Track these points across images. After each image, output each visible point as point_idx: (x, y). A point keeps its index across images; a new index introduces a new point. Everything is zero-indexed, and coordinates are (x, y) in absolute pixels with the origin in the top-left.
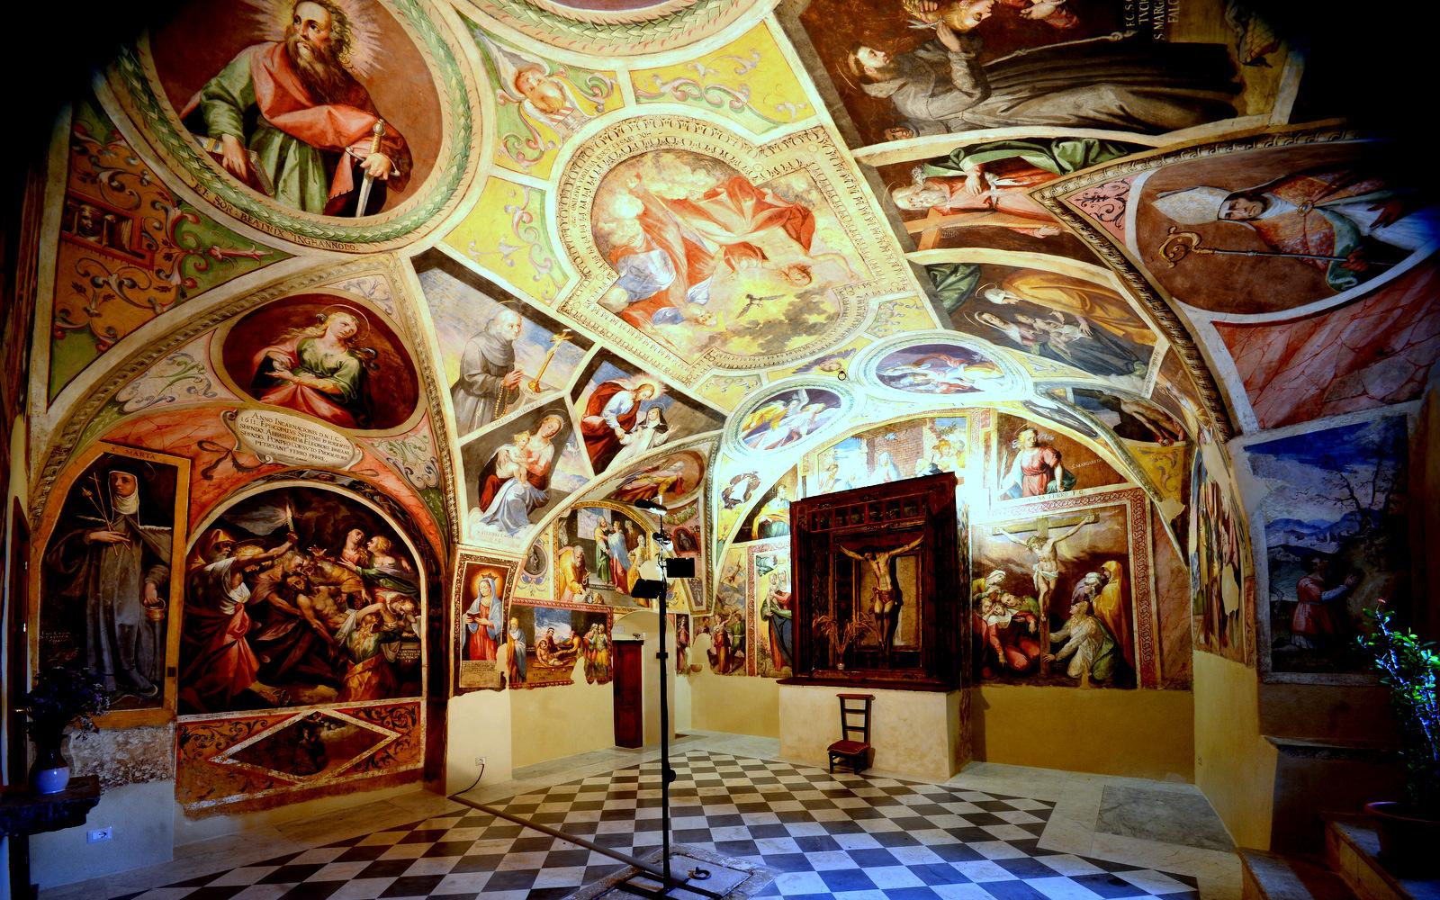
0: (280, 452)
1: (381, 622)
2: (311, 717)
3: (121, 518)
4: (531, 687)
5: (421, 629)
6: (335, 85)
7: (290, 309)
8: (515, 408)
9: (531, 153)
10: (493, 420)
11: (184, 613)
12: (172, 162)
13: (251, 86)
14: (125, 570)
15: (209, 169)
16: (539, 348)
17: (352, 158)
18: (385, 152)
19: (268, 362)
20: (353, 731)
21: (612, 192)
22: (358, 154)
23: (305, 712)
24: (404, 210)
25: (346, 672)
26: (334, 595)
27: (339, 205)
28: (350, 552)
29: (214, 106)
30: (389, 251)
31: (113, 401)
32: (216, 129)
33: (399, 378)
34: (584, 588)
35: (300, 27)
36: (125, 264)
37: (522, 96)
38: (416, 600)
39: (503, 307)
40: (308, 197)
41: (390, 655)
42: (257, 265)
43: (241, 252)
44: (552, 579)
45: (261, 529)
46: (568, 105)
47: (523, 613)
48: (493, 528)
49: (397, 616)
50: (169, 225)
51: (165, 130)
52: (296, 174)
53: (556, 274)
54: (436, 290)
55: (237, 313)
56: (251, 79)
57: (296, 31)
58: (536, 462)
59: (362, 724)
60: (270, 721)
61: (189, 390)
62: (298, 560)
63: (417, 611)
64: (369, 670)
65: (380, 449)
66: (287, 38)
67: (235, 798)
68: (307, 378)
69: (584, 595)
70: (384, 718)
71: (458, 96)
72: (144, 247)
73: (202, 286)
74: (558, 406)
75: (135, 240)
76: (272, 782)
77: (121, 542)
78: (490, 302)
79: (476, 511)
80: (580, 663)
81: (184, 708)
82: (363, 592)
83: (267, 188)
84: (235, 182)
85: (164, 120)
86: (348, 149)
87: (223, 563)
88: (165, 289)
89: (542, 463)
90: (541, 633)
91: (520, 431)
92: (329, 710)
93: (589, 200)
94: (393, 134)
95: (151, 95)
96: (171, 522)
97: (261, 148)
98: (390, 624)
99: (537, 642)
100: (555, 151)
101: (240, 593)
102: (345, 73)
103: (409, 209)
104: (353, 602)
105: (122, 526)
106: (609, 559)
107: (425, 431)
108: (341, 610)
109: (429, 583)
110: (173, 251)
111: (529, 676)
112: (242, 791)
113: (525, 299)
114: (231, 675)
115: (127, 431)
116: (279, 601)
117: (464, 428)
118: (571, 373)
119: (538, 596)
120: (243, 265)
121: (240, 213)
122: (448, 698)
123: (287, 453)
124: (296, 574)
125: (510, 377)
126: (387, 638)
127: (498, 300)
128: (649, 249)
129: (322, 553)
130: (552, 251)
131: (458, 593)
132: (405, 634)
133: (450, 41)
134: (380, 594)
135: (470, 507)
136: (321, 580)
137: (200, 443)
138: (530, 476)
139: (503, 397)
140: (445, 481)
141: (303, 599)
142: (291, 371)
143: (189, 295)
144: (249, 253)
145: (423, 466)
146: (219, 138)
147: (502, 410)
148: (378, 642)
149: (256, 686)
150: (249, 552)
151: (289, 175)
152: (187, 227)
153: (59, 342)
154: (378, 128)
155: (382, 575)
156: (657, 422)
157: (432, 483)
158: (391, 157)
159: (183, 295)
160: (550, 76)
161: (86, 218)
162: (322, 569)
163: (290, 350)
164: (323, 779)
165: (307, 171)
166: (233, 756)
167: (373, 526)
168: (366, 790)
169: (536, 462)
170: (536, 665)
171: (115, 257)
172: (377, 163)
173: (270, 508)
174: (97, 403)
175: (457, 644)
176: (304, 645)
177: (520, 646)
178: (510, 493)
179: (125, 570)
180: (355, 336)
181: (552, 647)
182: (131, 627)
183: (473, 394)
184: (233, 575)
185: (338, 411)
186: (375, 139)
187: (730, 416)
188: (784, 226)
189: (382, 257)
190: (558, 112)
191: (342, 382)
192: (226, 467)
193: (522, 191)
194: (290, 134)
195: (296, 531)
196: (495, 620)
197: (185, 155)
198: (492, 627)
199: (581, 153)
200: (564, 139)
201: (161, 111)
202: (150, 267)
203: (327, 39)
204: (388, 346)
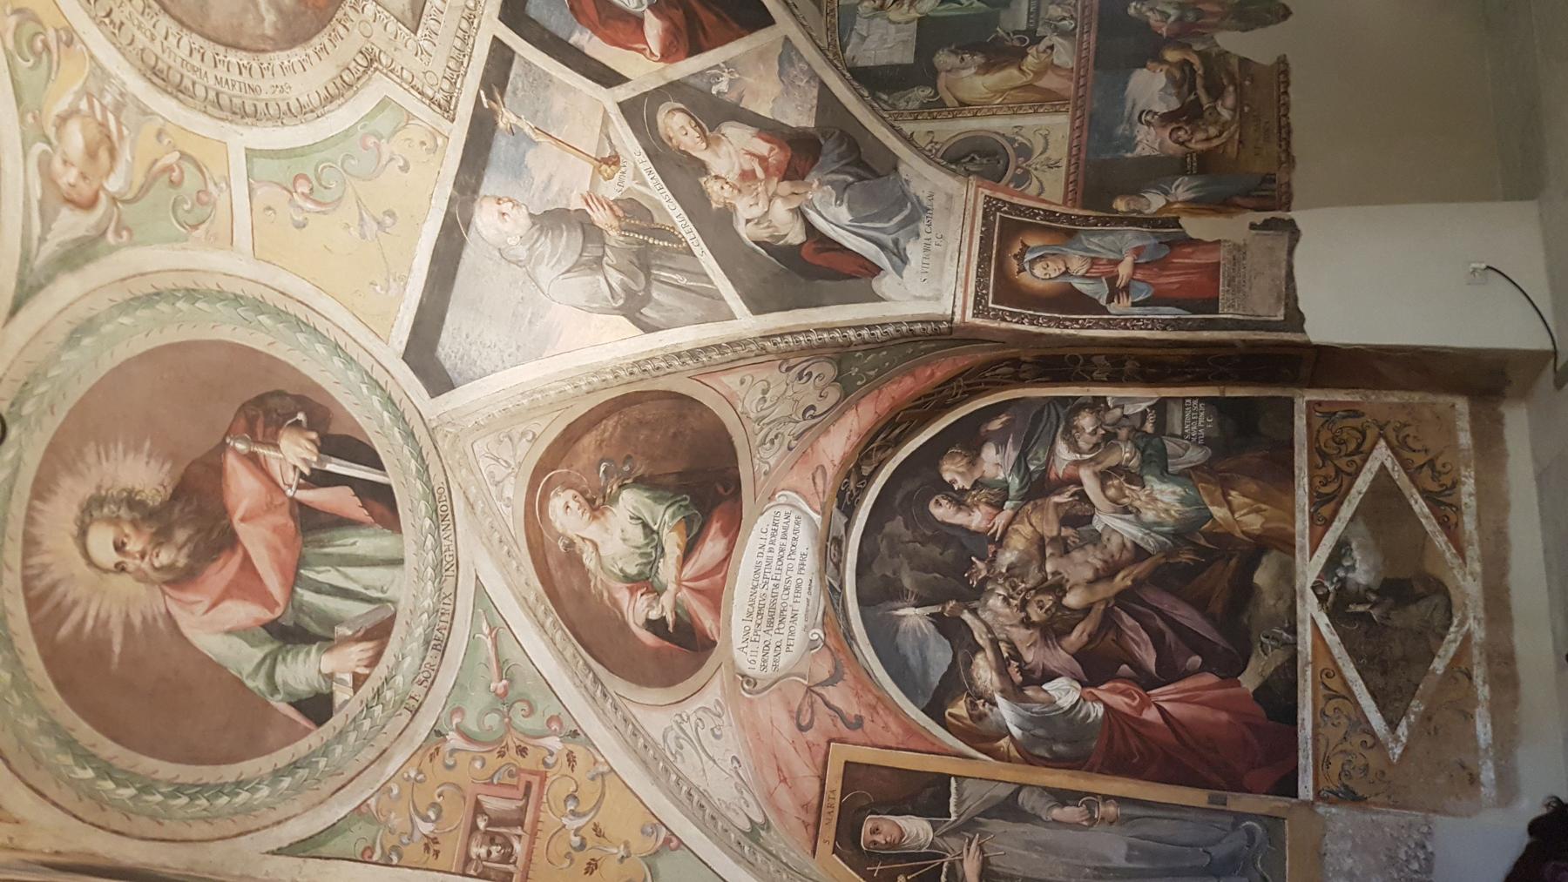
1: (1118, 470)
2: (1322, 599)
3: (938, 840)
4: (1290, 161)
5: (1138, 398)
7: (562, 590)
9: (191, 181)
11: (1099, 772)
12: (382, 742)
14: (1030, 845)
15: (378, 693)
18: (276, 436)
20: (1361, 527)
23: (1310, 610)
24: (362, 412)
25: (1230, 535)
26: (1065, 549)
27: (379, 508)
28: (976, 519)
29: (285, 683)
30: (431, 433)
31: (754, 833)
32: (320, 685)
33: (642, 423)
34: (1036, 40)
35: (131, 564)
36: (544, 807)
37: (102, 196)
38: (1076, 406)
39: (472, 233)
40: (380, 555)
41: (1196, 455)
42: (504, 632)
43: (492, 654)
44: (1018, 121)
45: (940, 656)
46: (84, 105)
47: (1102, 182)
48: (914, 250)
49: (1108, 439)
50: (475, 748)
51: (339, 749)
52: (352, 571)
53: (384, 123)
54: (474, 354)
55: (586, 663)
56: (229, 632)
57: (139, 569)
58: (763, 160)
59: (1346, 511)
60: (1324, 664)
61: (717, 737)
62: (995, 602)
63: (1097, 405)
64: (1225, 495)
65: (772, 461)
66: (153, 583)
67: (1483, 730)
68: (667, 571)
70: (1338, 471)
71: (144, 313)
72: (514, 781)
73: (555, 709)
74: (638, 113)
75: (506, 792)
76: (1460, 669)
77: (980, 846)
78: (469, 256)
79: (885, 284)
80: (1232, 42)
81: (1288, 786)
82: (1057, 499)
84: (388, 657)
85: (326, 750)
86: (290, 493)
87: (1006, 712)
88: (571, 759)
89: (763, 148)
90: (1149, 141)
91: (704, 197)
92: (1309, 568)
93: (234, 57)
94: (242, 422)
95: (294, 766)
96: (944, 779)
97: (331, 622)
98: (1125, 453)
99: (1173, 148)
100: (169, 128)
101: (1063, 692)
102: (175, 496)
103: (352, 398)
104: (1078, 518)
105: (953, 842)
107: (731, 381)
108: (1096, 539)
109: (1037, 381)
110: (511, 745)
111: (1259, 167)
112: (1469, 717)
114: (1223, 717)
115: (794, 823)
116: (1077, 636)
118: (568, 89)
119: (1059, 150)
120: (511, 652)
122: (1308, 346)
123: (801, 608)
124: (1024, 605)
125: (601, 217)
126: (1155, 460)
127: (462, 242)
129: (980, 565)
130: (347, 134)
131: (1059, 323)
132: (1149, 427)
134: (1060, 468)
136: (1034, 569)
137: (801, 728)
140: (823, 345)
141: (1072, 599)
143: (574, 727)
144: (489, 642)
145: (798, 386)
146: (330, 677)
147: (669, 234)
148: (1164, 474)
149: (1249, 681)
150: (984, 672)
151: (355, 581)
152: (472, 725)
154: (241, 446)
155: (1021, 464)
157: (830, 371)
158: (279, 427)
159: (575, 734)
160: (49, 143)
161: (489, 853)
163: (627, 593)
164: (1467, 584)
165: (341, 556)
166: (1392, 725)
167: (921, 477)
168: (1504, 507)
169: (763, 160)
170: (1232, 150)
171: (536, 821)
172: (294, 452)
173: (900, 639)
174: (759, 857)
175: (1176, 325)
176: (1167, 603)
177: (1182, 190)
178: (835, 218)
179: (1030, 845)
180: (583, 493)
181: (1186, 115)
182: (1131, 847)
184: (1028, 699)
185: (715, 527)
186: (262, 451)
189: (444, 446)
190: (103, 125)
191: (665, 517)
192: (835, 695)
194: (294, 580)
195: (942, 602)
196: (1123, 248)
197: (367, 724)
198: (1138, 251)
199: (155, 74)
200: (145, 112)
203: (134, 523)
204: (589, 441)
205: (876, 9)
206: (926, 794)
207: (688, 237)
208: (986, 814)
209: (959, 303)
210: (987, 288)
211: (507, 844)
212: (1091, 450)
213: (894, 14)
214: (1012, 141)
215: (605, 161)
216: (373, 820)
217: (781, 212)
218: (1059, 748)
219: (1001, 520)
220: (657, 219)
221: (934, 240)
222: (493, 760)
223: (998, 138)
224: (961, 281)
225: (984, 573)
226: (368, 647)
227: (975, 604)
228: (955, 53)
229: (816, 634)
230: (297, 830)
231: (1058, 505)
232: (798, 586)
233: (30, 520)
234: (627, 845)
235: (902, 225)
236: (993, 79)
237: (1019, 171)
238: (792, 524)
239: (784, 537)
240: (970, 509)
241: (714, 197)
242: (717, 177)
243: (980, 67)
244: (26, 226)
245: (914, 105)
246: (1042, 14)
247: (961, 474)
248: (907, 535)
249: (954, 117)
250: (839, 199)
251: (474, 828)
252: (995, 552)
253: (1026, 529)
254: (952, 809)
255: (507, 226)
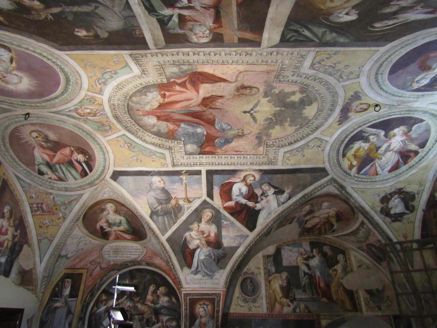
0: (116, 258)
6: (56, 146)
8: (183, 214)
10: (175, 223)
13: (43, 158)
16: (177, 184)
17: (75, 160)
18: (80, 154)
19: (102, 228)
21: (140, 120)
22: (75, 158)
26: (140, 320)
28: (149, 297)
30: (103, 179)
34: (292, 301)
39: (151, 177)
44: (264, 298)
48: (199, 276)
55: (79, 218)
58: (209, 235)
62: (129, 304)
69: (292, 307)
73: (67, 213)
74: (205, 204)
78: (146, 178)
79: (186, 270)
82: (153, 317)
83: (65, 179)
87: (103, 308)
88: (59, 219)
89: (213, 235)
91: (192, 223)
96: (77, 296)
106: (311, 277)
113: (157, 170)
117: (164, 231)
119: (254, 311)
120: (74, 203)
121: (64, 189)
123: (118, 258)
125: (173, 202)
127: (147, 175)
128: (179, 126)
129: (138, 299)
130: (149, 149)
133: (59, 119)
135: (182, 268)
136: (136, 312)
137: (91, 262)
138: (209, 243)
139: (174, 211)
142: (110, 227)
144: (73, 199)
146: (47, 174)
147: (177, 218)
152: (56, 199)
153: (40, 244)
155: (163, 307)
156: (272, 190)
159: (64, 218)
162: (137, 307)
171: (45, 215)
172: (81, 157)
178: (201, 255)
183: (160, 215)
185: (131, 236)
187: (327, 166)
188: (202, 83)
189: (103, 182)
192: (98, 269)
193: (119, 139)
194: (59, 163)
197: (44, 182)
201: (33, 175)
202: (53, 214)
203: (43, 138)
205: (301, 253)
206: (74, 294)
207: (178, 222)
208: (68, 307)
209: (187, 289)
210: (193, 296)
211: (38, 210)
212: (166, 325)
213: (300, 258)
214: (258, 297)
215: (188, 200)
216: (30, 187)
217: (197, 242)
218: (94, 322)
219: (149, 303)
220: (179, 214)
221: (204, 281)
222: (52, 204)
223: (259, 292)
224: (194, 289)
225: (136, 300)
226: (57, 178)
227: (128, 299)
228: (287, 277)
229: (112, 263)
230: (20, 175)
231: (152, 318)
232: (123, 257)
233: (26, 124)
234: (47, 232)
235: (204, 272)
236: (278, 289)
237: (248, 300)
238: (138, 253)
239: (135, 252)
240: (152, 295)
241: (193, 226)
242: (199, 226)
243: (282, 285)
244: (67, 109)
245: (269, 268)
246: (301, 302)
247: (161, 292)
248: (146, 280)
249: (265, 280)
250: (206, 256)
251: (38, 204)
252: (140, 302)
253: (146, 310)
254: (70, 299)
255: (158, 183)
